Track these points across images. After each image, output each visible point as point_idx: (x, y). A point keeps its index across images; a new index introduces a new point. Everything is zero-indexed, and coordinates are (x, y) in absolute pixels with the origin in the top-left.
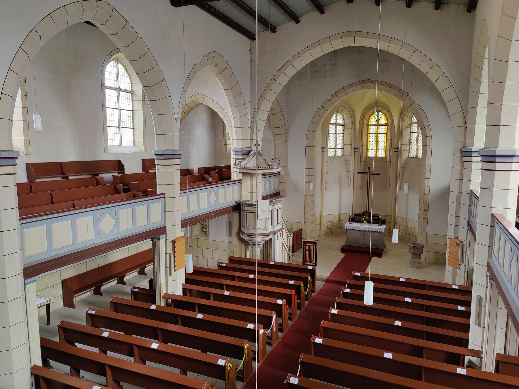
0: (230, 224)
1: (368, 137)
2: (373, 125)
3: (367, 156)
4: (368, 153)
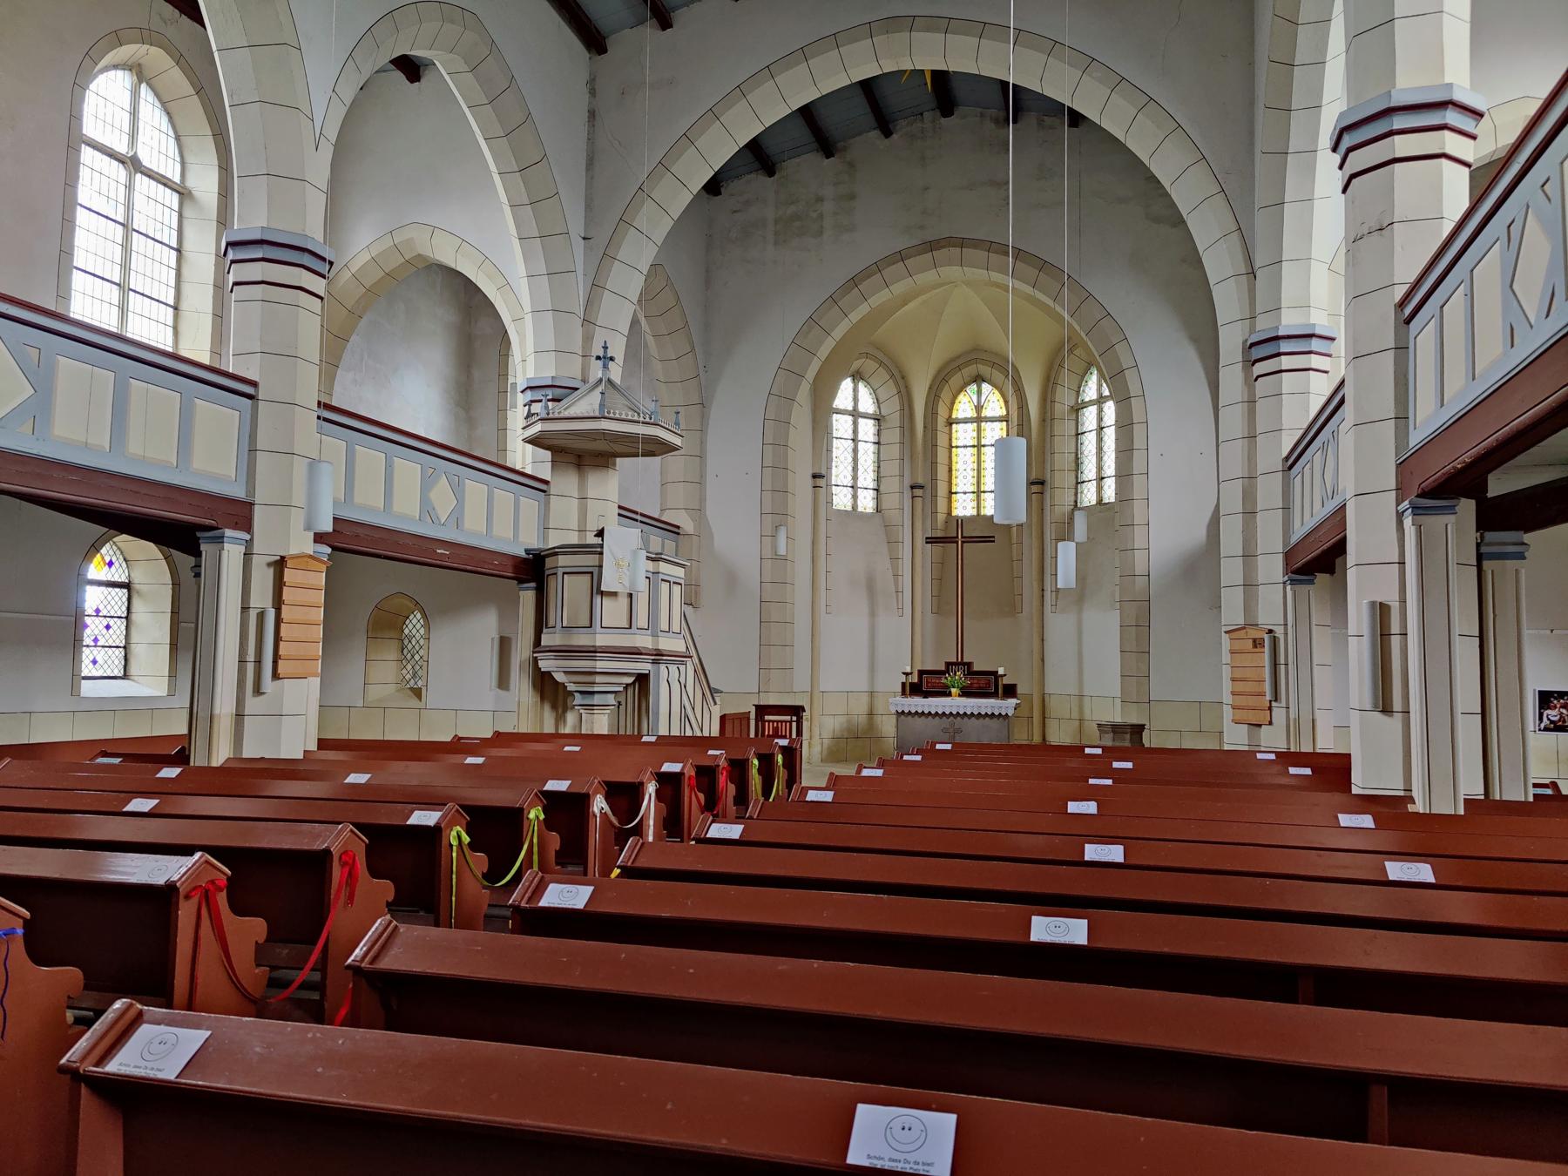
0: (504, 645)
1: (950, 458)
2: (966, 421)
3: (949, 513)
4: (954, 505)
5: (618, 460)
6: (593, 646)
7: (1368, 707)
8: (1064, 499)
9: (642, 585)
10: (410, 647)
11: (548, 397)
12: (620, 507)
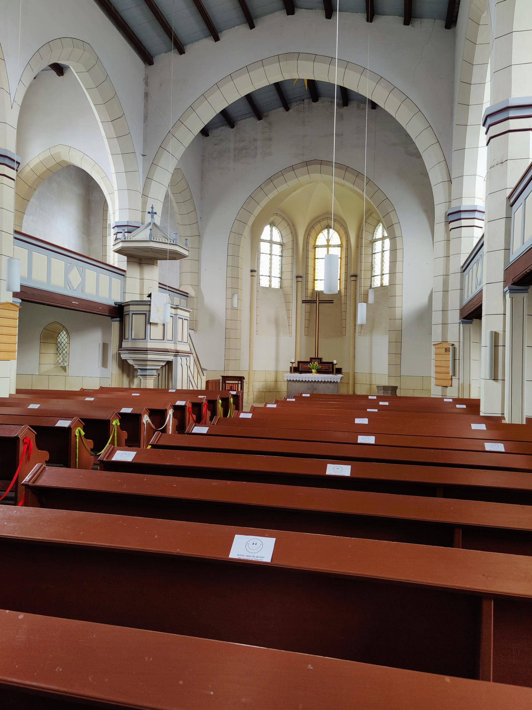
0: (105, 347)
2: (322, 246)
3: (314, 289)
4: (316, 285)
5: (159, 261)
6: (146, 348)
7: (488, 377)
8: (364, 283)
9: (169, 320)
10: (61, 347)
11: (125, 231)
12: (159, 283)
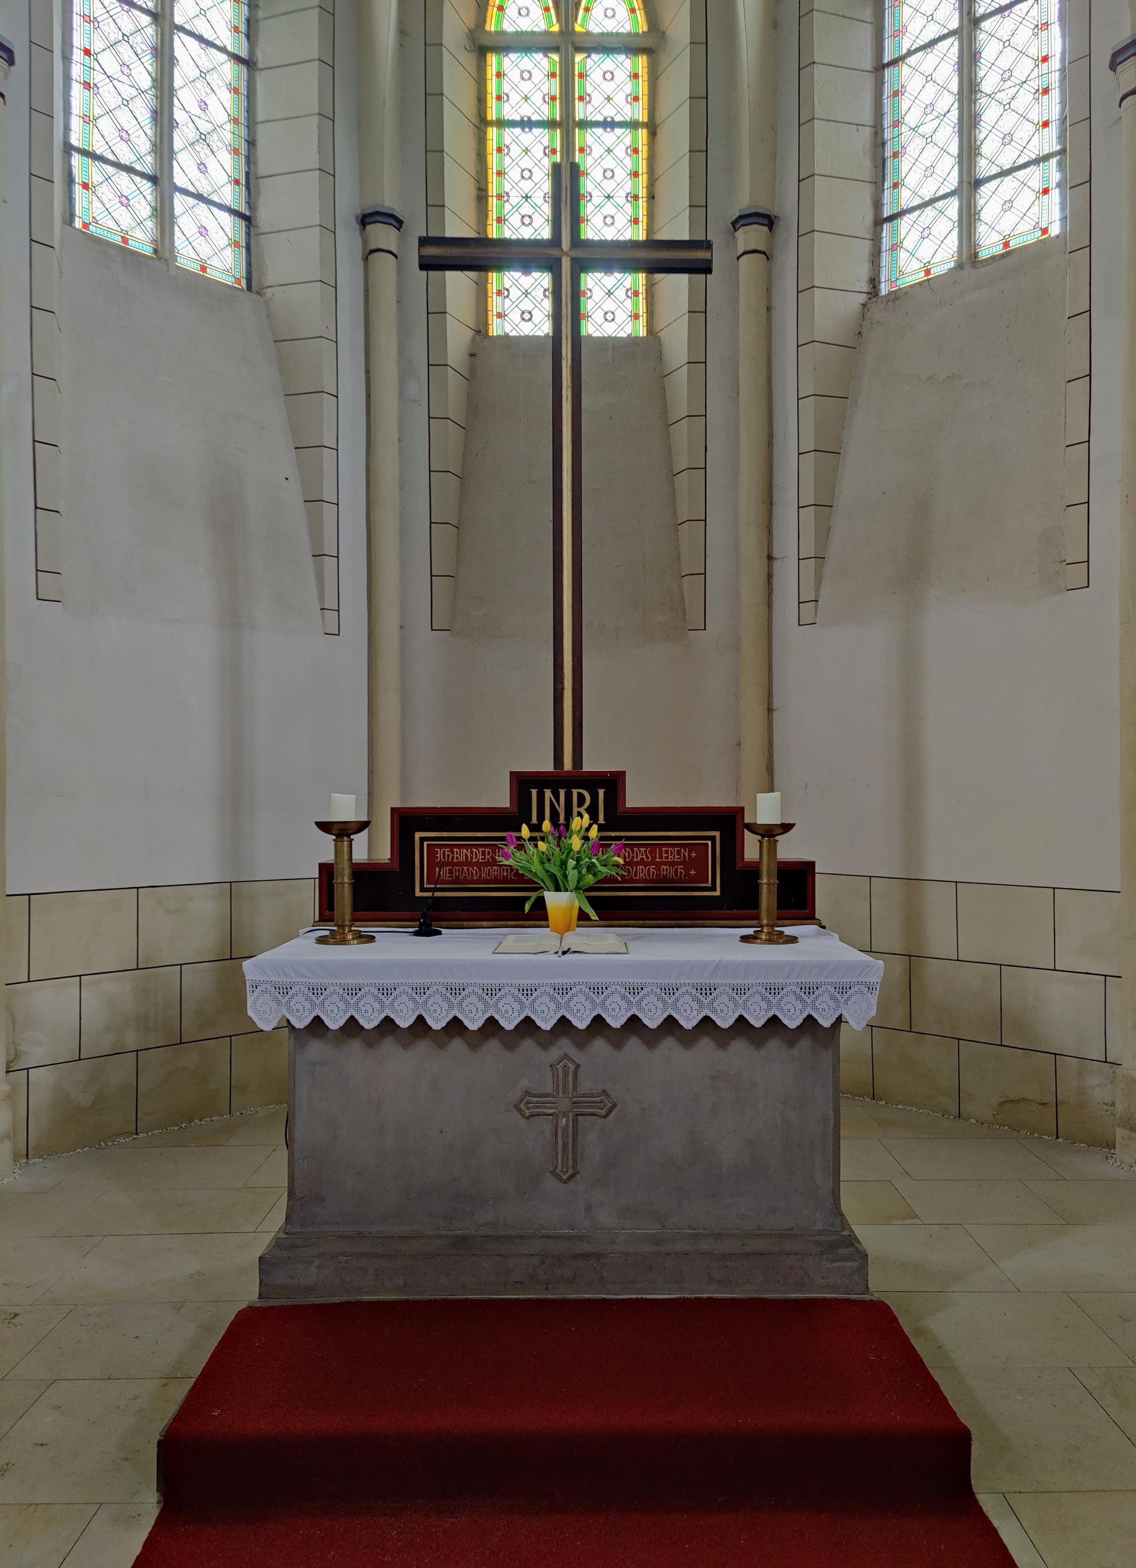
1: (481, 156)
2: (526, 43)
3: (481, 330)
4: (495, 304)
